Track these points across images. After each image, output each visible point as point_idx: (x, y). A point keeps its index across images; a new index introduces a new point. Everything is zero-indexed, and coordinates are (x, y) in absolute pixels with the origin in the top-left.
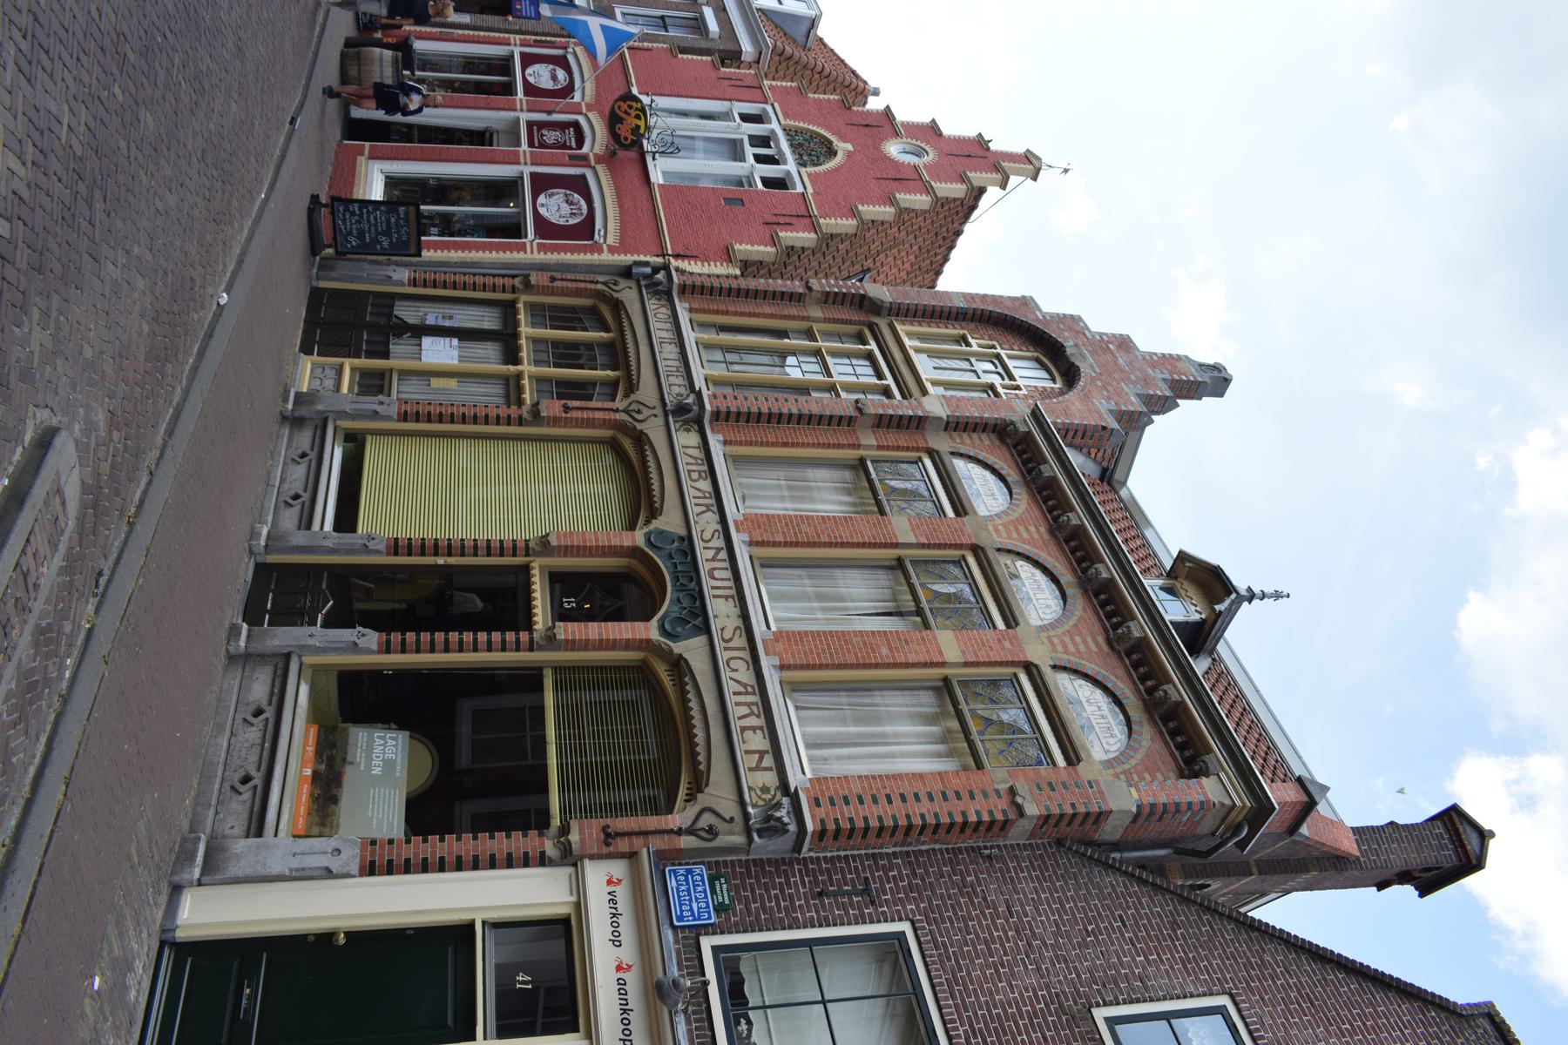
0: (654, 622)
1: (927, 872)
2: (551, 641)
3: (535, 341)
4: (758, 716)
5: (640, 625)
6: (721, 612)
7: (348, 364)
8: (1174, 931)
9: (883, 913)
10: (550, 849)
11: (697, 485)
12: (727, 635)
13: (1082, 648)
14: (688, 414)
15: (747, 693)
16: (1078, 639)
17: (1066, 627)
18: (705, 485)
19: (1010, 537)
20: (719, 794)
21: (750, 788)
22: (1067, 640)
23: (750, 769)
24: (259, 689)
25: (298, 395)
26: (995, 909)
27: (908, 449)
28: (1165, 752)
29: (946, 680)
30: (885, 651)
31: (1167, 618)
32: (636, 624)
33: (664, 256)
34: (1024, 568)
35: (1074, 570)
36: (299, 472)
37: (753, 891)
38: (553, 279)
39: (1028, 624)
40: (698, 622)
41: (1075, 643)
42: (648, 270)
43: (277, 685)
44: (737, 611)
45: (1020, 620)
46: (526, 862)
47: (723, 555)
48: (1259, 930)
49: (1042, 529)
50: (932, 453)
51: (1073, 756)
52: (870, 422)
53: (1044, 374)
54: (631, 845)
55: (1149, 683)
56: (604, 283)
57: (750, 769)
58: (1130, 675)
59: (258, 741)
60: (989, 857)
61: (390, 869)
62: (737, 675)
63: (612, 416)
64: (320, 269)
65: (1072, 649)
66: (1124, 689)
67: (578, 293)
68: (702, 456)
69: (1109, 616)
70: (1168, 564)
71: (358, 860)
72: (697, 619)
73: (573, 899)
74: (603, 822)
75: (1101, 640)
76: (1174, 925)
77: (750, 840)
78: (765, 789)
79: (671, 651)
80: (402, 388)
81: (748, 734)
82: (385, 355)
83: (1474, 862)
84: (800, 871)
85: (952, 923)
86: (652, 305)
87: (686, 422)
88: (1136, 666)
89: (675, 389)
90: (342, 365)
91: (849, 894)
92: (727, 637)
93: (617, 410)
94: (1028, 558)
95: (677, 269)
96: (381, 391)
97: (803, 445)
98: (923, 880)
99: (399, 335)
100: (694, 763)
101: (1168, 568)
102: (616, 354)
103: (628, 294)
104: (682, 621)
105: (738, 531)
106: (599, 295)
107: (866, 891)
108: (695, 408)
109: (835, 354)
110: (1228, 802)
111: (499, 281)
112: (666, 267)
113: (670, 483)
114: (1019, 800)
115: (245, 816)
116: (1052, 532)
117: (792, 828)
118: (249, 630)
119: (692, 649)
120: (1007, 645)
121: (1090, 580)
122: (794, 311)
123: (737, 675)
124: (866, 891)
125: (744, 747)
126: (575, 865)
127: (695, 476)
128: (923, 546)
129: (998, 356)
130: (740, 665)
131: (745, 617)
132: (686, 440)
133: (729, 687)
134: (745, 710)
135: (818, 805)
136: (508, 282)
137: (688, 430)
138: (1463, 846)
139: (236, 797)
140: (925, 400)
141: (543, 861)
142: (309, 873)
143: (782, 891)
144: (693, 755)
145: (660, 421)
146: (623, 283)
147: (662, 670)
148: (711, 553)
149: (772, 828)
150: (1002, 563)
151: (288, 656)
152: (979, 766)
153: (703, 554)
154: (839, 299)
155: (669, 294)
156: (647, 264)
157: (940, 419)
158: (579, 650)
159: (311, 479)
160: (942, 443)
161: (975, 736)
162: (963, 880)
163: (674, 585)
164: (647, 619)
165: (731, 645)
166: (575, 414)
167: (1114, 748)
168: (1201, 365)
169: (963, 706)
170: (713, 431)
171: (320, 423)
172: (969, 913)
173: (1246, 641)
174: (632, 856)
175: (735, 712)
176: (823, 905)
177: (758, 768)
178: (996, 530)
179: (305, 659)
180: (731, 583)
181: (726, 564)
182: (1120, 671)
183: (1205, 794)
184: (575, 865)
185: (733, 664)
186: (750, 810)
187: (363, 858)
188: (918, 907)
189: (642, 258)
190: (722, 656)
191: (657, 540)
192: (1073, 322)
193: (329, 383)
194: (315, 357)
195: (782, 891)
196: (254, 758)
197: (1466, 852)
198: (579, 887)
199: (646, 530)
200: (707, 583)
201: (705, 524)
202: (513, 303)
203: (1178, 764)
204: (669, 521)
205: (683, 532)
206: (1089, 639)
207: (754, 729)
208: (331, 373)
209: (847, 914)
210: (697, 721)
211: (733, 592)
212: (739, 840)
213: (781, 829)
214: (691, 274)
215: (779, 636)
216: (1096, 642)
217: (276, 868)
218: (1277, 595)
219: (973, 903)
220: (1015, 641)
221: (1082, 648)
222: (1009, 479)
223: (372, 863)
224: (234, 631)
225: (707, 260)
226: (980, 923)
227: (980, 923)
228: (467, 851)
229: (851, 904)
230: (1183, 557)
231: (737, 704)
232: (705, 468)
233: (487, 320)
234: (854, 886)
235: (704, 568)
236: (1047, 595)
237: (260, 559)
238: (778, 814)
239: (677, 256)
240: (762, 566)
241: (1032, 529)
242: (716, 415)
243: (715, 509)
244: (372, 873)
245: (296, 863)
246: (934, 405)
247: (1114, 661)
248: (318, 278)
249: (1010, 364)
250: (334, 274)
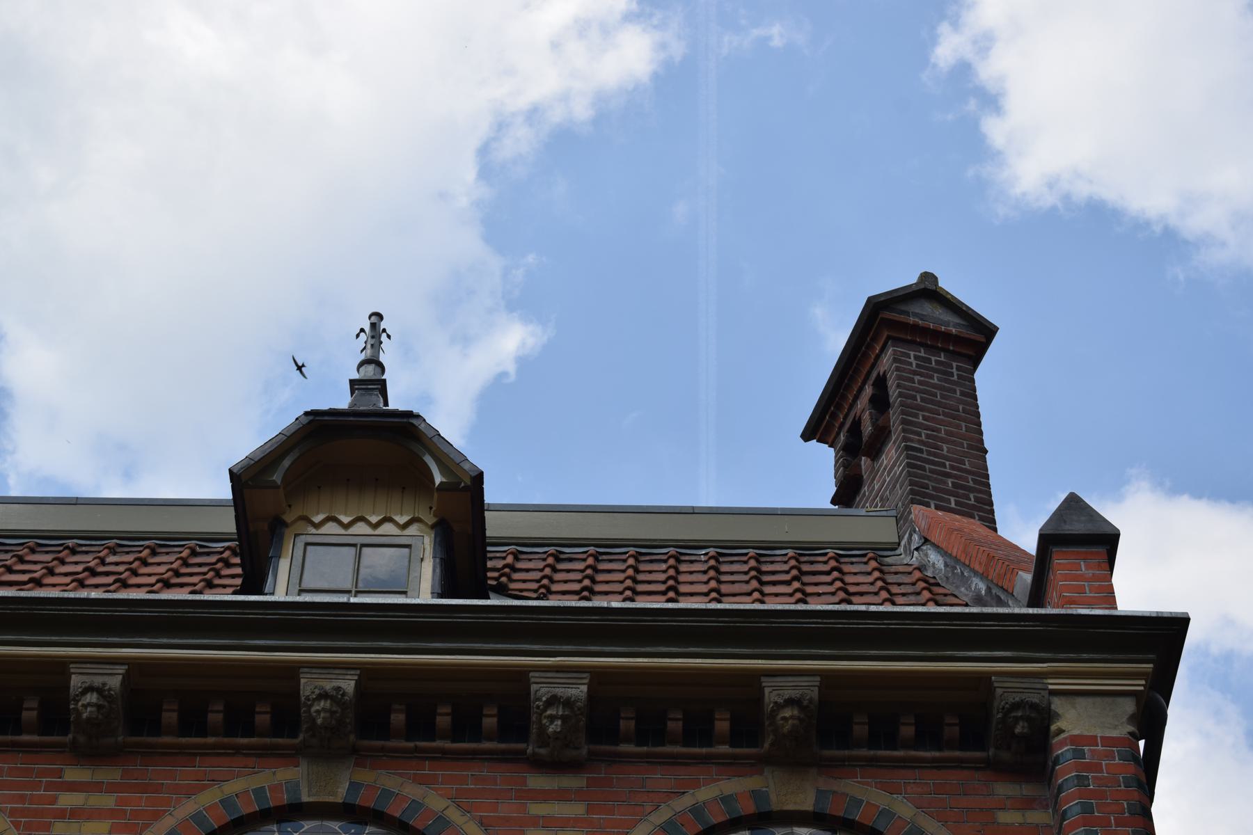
75: (537, 782)
182: (659, 778)
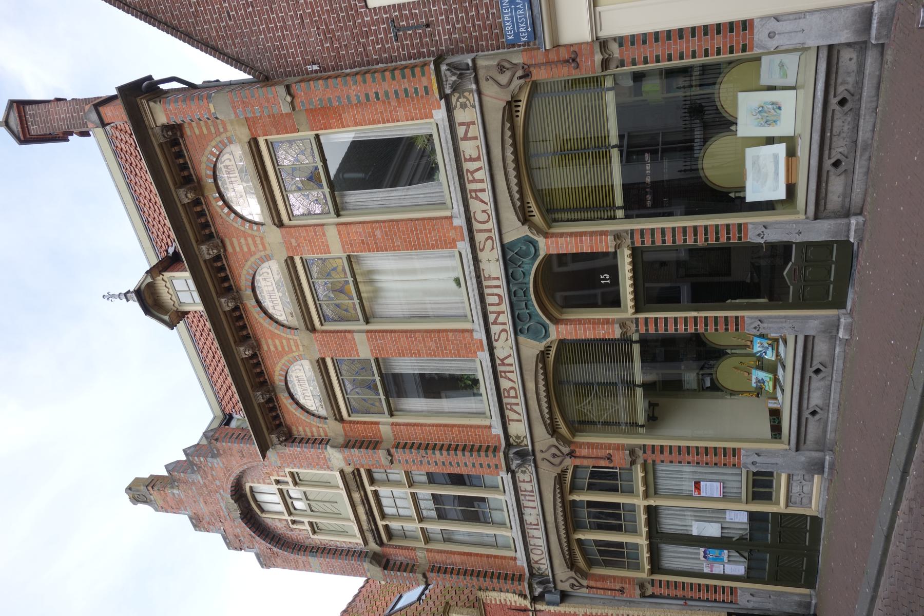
0: (542, 253)
1: (356, 49)
2: (617, 236)
3: (634, 531)
4: (468, 171)
5: (564, 336)
6: (493, 267)
7: (780, 507)
8: (196, 10)
9: (386, 13)
10: (614, 47)
11: (511, 384)
12: (504, 335)
13: (243, 241)
14: (518, 454)
15: (505, 372)
16: (245, 250)
17: (253, 259)
18: (505, 384)
19: (288, 340)
21: (474, 106)
22: (253, 249)
23: (473, 123)
24: (836, 185)
25: (821, 471)
26: (311, 20)
27: (358, 422)
28: (192, 152)
29: (367, 322)
30: (378, 233)
31: (187, 274)
32: (555, 252)
33: (535, 610)
34: (282, 318)
35: (245, 310)
36: (816, 399)
37: (474, 25)
38: (622, 591)
39: (279, 263)
40: (510, 254)
41: (248, 245)
42: (548, 597)
43: (823, 190)
44: (482, 266)
45: (284, 265)
46: (633, 39)
47: (492, 318)
48: (142, 13)
49: (265, 348)
50: (341, 420)
51: (321, 364)
52: (384, 445)
53: (261, 498)
54: (558, 55)
55: (271, 405)
56: (582, 586)
57: (473, 123)
58: (212, 218)
59: (835, 139)
60: (314, 63)
61: (731, 26)
62: (481, 208)
63: (592, 584)
64: (810, 603)
65: (250, 240)
66: (254, 311)
67: (603, 578)
68: (508, 413)
69: (223, 269)
70: (181, 324)
71: (755, 31)
72: (511, 256)
73: (598, 9)
75: (230, 249)
76: (196, 15)
77: (474, 60)
78: (464, 106)
79: (530, 228)
80: (737, 485)
81: (475, 155)
82: (752, 516)
83: (15, 105)
84: (441, 44)
85: (340, 7)
86: (544, 566)
87: (542, 575)
88: (226, 279)
89: (526, 477)
90: (787, 506)
91: (409, 28)
92: (490, 242)
93: (588, 587)
94: (277, 322)
95: (525, 597)
96: (755, 474)
97: (433, 425)
98: (359, 42)
99: (741, 538)
100: (545, 368)
101: (181, 322)
102: (572, 517)
103: (563, 573)
104: (525, 255)
105: (481, 341)
106: (585, 575)
107: (397, 29)
108: (511, 455)
109: (408, 518)
110: (152, 104)
111: (664, 591)
112: (534, 600)
113: (531, 385)
114: (289, 99)
115: (841, 71)
116: (259, 345)
117: (444, 68)
118: (848, 237)
119: (515, 231)
120: (294, 242)
121: (234, 299)
122: (438, 557)
123: (481, 208)
124: (397, 29)
125: (477, 143)
126: (597, 39)
127: (512, 393)
128: (349, 332)
129: (290, 514)
130: (481, 217)
131: (476, 260)
132: (518, 429)
133: (487, 196)
134: (515, 407)
135: (426, 88)
136: (658, 591)
137: (518, 437)
138: (20, 116)
139: (850, 87)
140: (342, 464)
141: (620, 41)
142: (791, 17)
143: (454, 26)
144: (545, 374)
145: (537, 448)
146: (565, 587)
147: (564, 430)
148: (502, 319)
149: (460, 70)
150: (294, 321)
151: (816, 217)
152: (349, 257)
153: (506, 318)
154: (403, 567)
155: (532, 575)
156: (549, 604)
157: (332, 447)
158: (597, 232)
159: (810, 347)
160: (333, 428)
161: (351, 280)
162: (332, 43)
163: (528, 289)
164: (549, 258)
165: (487, 235)
166: (602, 453)
167: (297, 367)
168: (145, 502)
169: (357, 302)
170: (499, 436)
171: (802, 446)
172: (329, 16)
173: (136, 264)
174: (556, 46)
175: (483, 174)
176: (426, 17)
177: (499, 313)
178: (297, 346)
179: (787, 447)
180: (487, 291)
181: (490, 309)
182: (218, 222)
183: (165, 110)
184: (597, 39)
185: (483, 217)
186: (474, 87)
187: (752, 33)
188: (363, 19)
189: (552, 609)
190: (492, 224)
191: (540, 332)
192: (233, 543)
193: (796, 489)
194: (807, 512)
195: (454, 26)
196: (837, 123)
197: (19, 112)
198: (595, 21)
199: (549, 340)
200: (503, 291)
201: (505, 347)
202: (653, 571)
203: (184, 141)
204: (532, 348)
205: (521, 338)
206: (238, 249)
207: (471, 159)
208: (795, 498)
209: (410, 11)
210: (511, 166)
211: (485, 283)
212: (481, 63)
213: (452, 67)
214: (514, 592)
215: (452, 244)
216: (233, 248)
217: (816, 18)
218: (109, 297)
219: (326, 25)
220: (288, 246)
221: (243, 241)
222: (287, 395)
223: (744, 29)
224: (860, 231)
225: (502, 606)
226: (322, 8)
227: (322, 8)
228: (675, 44)
229: (407, 19)
230: (171, 325)
231: (482, 181)
232: (505, 401)
233: (674, 556)
234: (405, 34)
235: (505, 307)
236: (265, 289)
237: (843, 311)
238: (454, 78)
239: (525, 610)
240: (484, 413)
241: (272, 348)
242: (496, 449)
243: (498, 362)
244: (744, 22)
245: (802, 23)
246: (336, 457)
247: (222, 230)
248: (811, 596)
249: (281, 508)
250: (797, 599)
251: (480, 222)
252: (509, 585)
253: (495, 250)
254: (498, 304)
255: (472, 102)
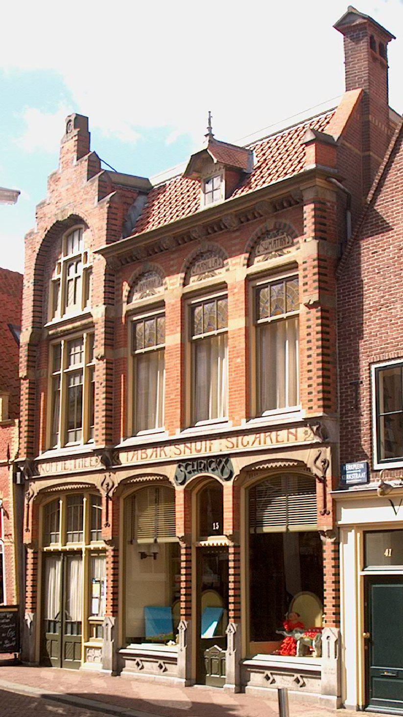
7: (84, 644)
20: (307, 457)
23: (296, 439)
74: (103, 526)
119: (237, 465)
198: (350, 527)
204: (170, 472)
239: (9, 457)
251: (242, 439)
252: (24, 445)
253: (226, 449)
254: (242, 444)
255: (308, 439)
